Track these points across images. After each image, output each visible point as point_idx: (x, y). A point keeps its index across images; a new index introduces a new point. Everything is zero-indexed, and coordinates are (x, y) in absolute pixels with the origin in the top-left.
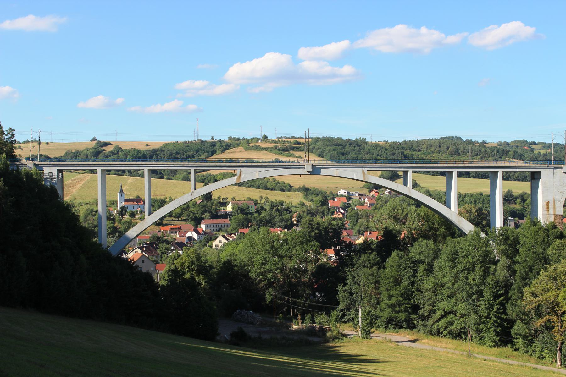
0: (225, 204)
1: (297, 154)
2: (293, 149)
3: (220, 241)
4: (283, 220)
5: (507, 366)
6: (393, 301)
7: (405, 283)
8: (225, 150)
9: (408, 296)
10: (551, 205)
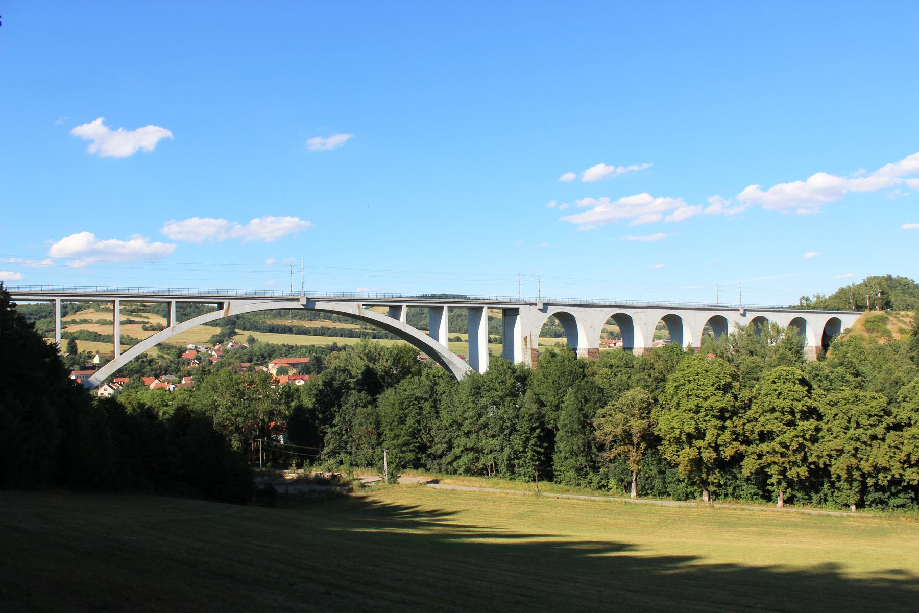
0: (91, 357)
1: (144, 314)
2: (140, 310)
3: (105, 390)
4: (152, 370)
5: (590, 503)
6: (401, 441)
7: (410, 421)
8: (76, 311)
9: (415, 434)
10: (528, 340)
